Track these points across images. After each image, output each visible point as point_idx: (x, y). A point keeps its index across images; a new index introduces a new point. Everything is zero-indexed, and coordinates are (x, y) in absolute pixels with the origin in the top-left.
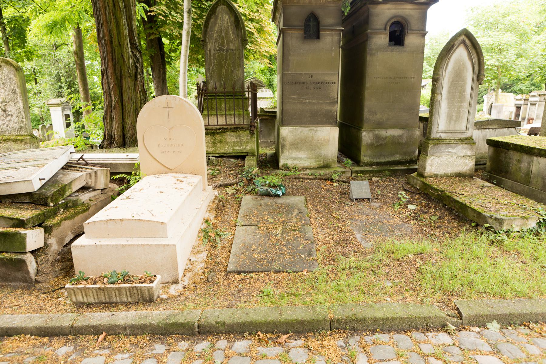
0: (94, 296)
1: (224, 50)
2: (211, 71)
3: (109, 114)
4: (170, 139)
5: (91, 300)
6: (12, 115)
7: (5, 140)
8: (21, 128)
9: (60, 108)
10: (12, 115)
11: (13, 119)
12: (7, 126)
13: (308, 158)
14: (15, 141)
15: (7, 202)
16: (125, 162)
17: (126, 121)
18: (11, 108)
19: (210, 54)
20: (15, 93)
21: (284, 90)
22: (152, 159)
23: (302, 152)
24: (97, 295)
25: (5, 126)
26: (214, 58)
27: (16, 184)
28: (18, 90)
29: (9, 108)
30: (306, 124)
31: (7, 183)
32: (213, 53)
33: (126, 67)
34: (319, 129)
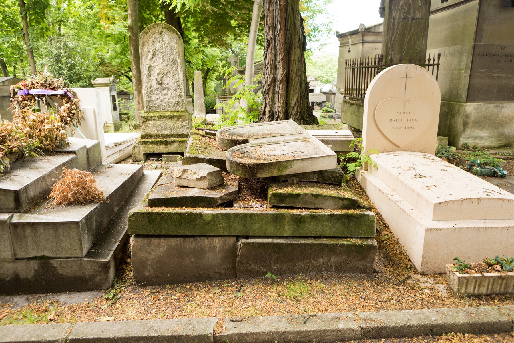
0: (488, 286)
1: (409, 18)
2: (392, 42)
3: (272, 88)
4: (404, 113)
5: (483, 290)
6: (168, 89)
7: (160, 117)
8: (178, 103)
9: (108, 88)
10: (168, 89)
11: (169, 93)
12: (162, 101)
13: (489, 137)
14: (172, 117)
15: (295, 181)
16: (338, 139)
17: (291, 96)
18: (168, 81)
19: (394, 22)
20: (174, 64)
21: (474, 63)
22: (380, 135)
23: (484, 130)
24: (493, 285)
25: (159, 101)
26: (398, 27)
27: (320, 159)
28: (179, 60)
29: (166, 81)
30: (492, 100)
31: (311, 158)
32: (397, 21)
33: (297, 36)
34: (505, 105)
